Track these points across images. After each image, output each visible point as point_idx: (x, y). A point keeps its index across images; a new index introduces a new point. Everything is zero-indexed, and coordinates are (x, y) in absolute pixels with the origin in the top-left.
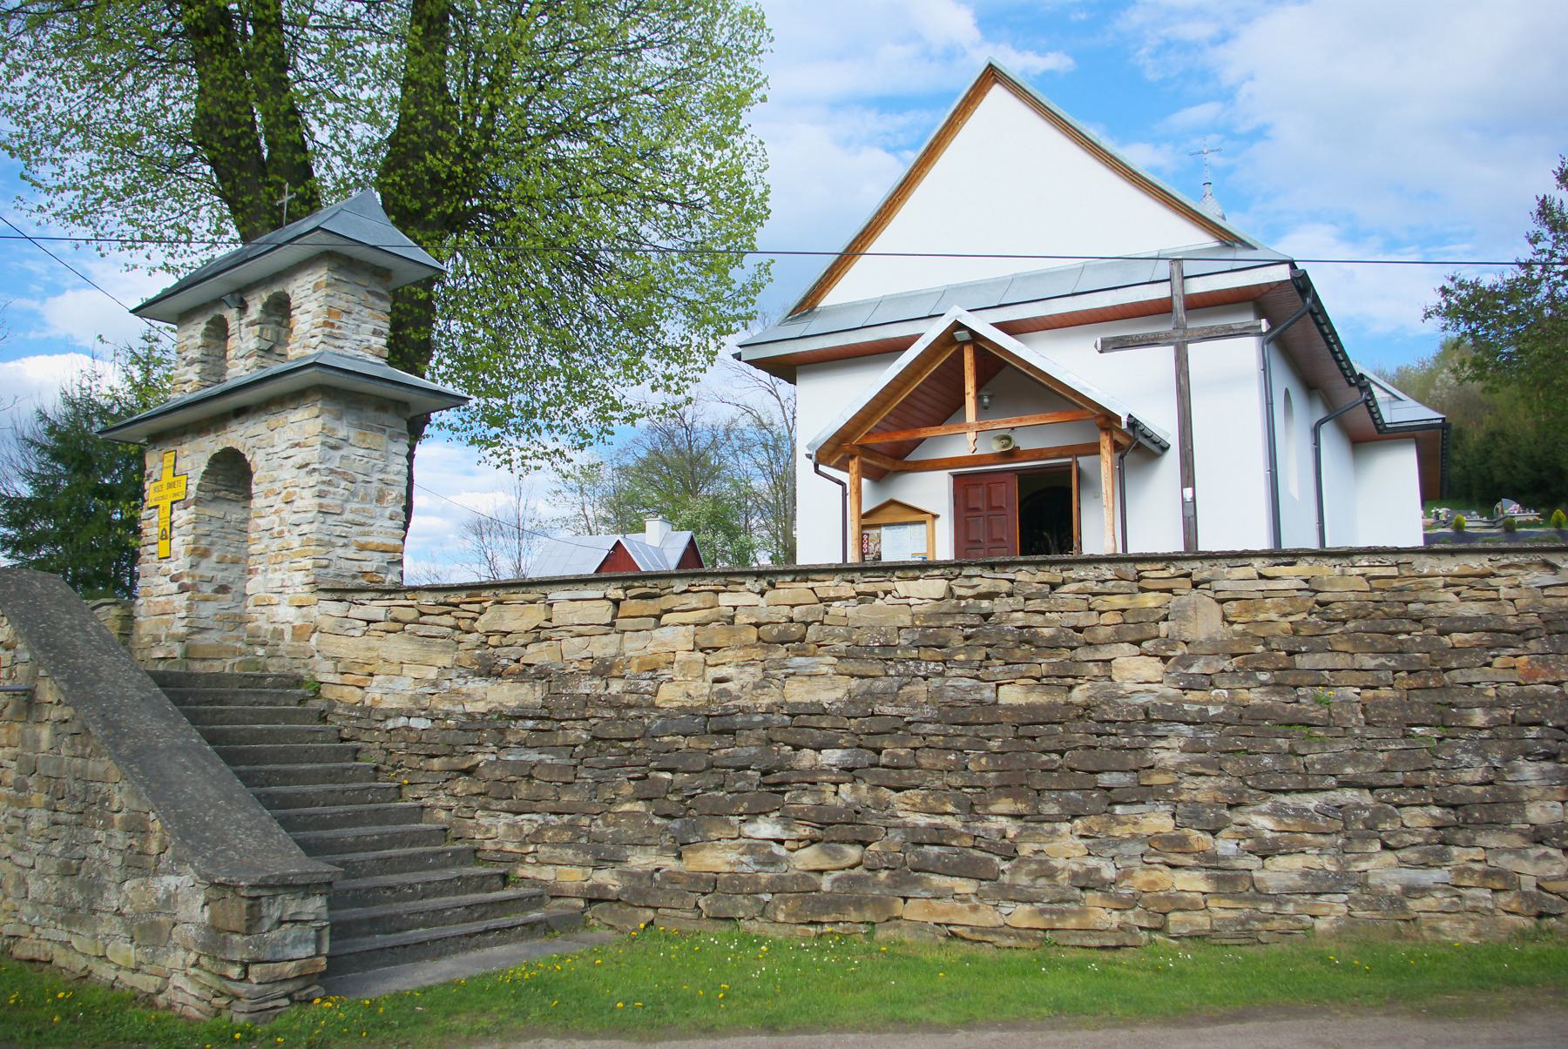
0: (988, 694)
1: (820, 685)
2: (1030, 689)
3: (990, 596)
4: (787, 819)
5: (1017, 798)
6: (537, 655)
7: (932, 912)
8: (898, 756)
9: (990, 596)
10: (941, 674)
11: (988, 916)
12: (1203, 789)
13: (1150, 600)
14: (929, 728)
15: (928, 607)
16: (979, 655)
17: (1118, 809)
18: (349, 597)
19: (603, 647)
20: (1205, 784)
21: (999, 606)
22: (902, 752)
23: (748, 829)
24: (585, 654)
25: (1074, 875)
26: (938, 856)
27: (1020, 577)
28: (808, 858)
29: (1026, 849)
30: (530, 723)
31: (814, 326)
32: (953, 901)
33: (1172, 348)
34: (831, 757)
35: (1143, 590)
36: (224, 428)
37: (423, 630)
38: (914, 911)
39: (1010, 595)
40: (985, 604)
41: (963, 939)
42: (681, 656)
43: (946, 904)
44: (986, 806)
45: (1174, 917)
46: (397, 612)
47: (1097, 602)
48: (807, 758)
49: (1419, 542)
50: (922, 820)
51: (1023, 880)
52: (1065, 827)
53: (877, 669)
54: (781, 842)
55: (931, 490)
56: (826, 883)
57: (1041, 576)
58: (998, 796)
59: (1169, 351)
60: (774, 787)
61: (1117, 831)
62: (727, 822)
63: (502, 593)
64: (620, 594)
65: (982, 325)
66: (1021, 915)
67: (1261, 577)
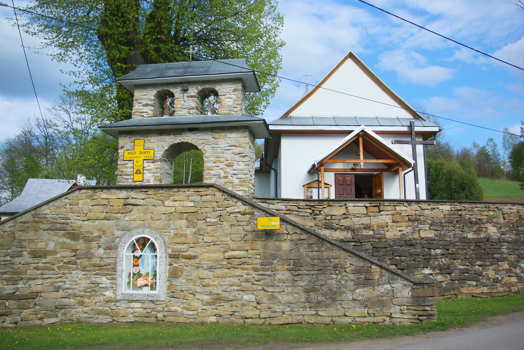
0: (465, 235)
1: (428, 233)
2: (474, 234)
3: (460, 210)
4: (433, 268)
5: (481, 261)
6: (343, 222)
7: (468, 290)
8: (453, 251)
9: (460, 210)
10: (454, 230)
11: (479, 291)
12: (512, 258)
13: (491, 213)
14: (458, 244)
15: (446, 213)
16: (461, 226)
17: (499, 263)
18: (268, 201)
19: (365, 221)
20: (512, 257)
21: (463, 213)
22: (454, 250)
23: (423, 272)
24: (361, 223)
25: (494, 279)
26: (468, 276)
27: (466, 206)
28: (439, 278)
29: (484, 273)
30: (353, 243)
31: (288, 122)
32: (470, 288)
33: (417, 145)
34: (439, 251)
35: (490, 210)
36: (181, 134)
37: (301, 214)
38: (464, 290)
39: (464, 210)
40: (460, 212)
41: (476, 297)
42: (389, 224)
43: (471, 288)
44: (475, 263)
45: (512, 288)
46: (289, 207)
47: (482, 213)
48: (433, 252)
49: (302, 198)
50: (462, 267)
51: (485, 281)
52: (490, 268)
53: (440, 228)
54: (431, 274)
55: (329, 178)
56: (444, 285)
57: (470, 206)
58: (477, 260)
59: (410, 146)
60: (427, 261)
61: (500, 268)
62: (418, 270)
63: (331, 203)
64: (369, 205)
65: (369, 131)
66: (485, 290)
67: (510, 209)
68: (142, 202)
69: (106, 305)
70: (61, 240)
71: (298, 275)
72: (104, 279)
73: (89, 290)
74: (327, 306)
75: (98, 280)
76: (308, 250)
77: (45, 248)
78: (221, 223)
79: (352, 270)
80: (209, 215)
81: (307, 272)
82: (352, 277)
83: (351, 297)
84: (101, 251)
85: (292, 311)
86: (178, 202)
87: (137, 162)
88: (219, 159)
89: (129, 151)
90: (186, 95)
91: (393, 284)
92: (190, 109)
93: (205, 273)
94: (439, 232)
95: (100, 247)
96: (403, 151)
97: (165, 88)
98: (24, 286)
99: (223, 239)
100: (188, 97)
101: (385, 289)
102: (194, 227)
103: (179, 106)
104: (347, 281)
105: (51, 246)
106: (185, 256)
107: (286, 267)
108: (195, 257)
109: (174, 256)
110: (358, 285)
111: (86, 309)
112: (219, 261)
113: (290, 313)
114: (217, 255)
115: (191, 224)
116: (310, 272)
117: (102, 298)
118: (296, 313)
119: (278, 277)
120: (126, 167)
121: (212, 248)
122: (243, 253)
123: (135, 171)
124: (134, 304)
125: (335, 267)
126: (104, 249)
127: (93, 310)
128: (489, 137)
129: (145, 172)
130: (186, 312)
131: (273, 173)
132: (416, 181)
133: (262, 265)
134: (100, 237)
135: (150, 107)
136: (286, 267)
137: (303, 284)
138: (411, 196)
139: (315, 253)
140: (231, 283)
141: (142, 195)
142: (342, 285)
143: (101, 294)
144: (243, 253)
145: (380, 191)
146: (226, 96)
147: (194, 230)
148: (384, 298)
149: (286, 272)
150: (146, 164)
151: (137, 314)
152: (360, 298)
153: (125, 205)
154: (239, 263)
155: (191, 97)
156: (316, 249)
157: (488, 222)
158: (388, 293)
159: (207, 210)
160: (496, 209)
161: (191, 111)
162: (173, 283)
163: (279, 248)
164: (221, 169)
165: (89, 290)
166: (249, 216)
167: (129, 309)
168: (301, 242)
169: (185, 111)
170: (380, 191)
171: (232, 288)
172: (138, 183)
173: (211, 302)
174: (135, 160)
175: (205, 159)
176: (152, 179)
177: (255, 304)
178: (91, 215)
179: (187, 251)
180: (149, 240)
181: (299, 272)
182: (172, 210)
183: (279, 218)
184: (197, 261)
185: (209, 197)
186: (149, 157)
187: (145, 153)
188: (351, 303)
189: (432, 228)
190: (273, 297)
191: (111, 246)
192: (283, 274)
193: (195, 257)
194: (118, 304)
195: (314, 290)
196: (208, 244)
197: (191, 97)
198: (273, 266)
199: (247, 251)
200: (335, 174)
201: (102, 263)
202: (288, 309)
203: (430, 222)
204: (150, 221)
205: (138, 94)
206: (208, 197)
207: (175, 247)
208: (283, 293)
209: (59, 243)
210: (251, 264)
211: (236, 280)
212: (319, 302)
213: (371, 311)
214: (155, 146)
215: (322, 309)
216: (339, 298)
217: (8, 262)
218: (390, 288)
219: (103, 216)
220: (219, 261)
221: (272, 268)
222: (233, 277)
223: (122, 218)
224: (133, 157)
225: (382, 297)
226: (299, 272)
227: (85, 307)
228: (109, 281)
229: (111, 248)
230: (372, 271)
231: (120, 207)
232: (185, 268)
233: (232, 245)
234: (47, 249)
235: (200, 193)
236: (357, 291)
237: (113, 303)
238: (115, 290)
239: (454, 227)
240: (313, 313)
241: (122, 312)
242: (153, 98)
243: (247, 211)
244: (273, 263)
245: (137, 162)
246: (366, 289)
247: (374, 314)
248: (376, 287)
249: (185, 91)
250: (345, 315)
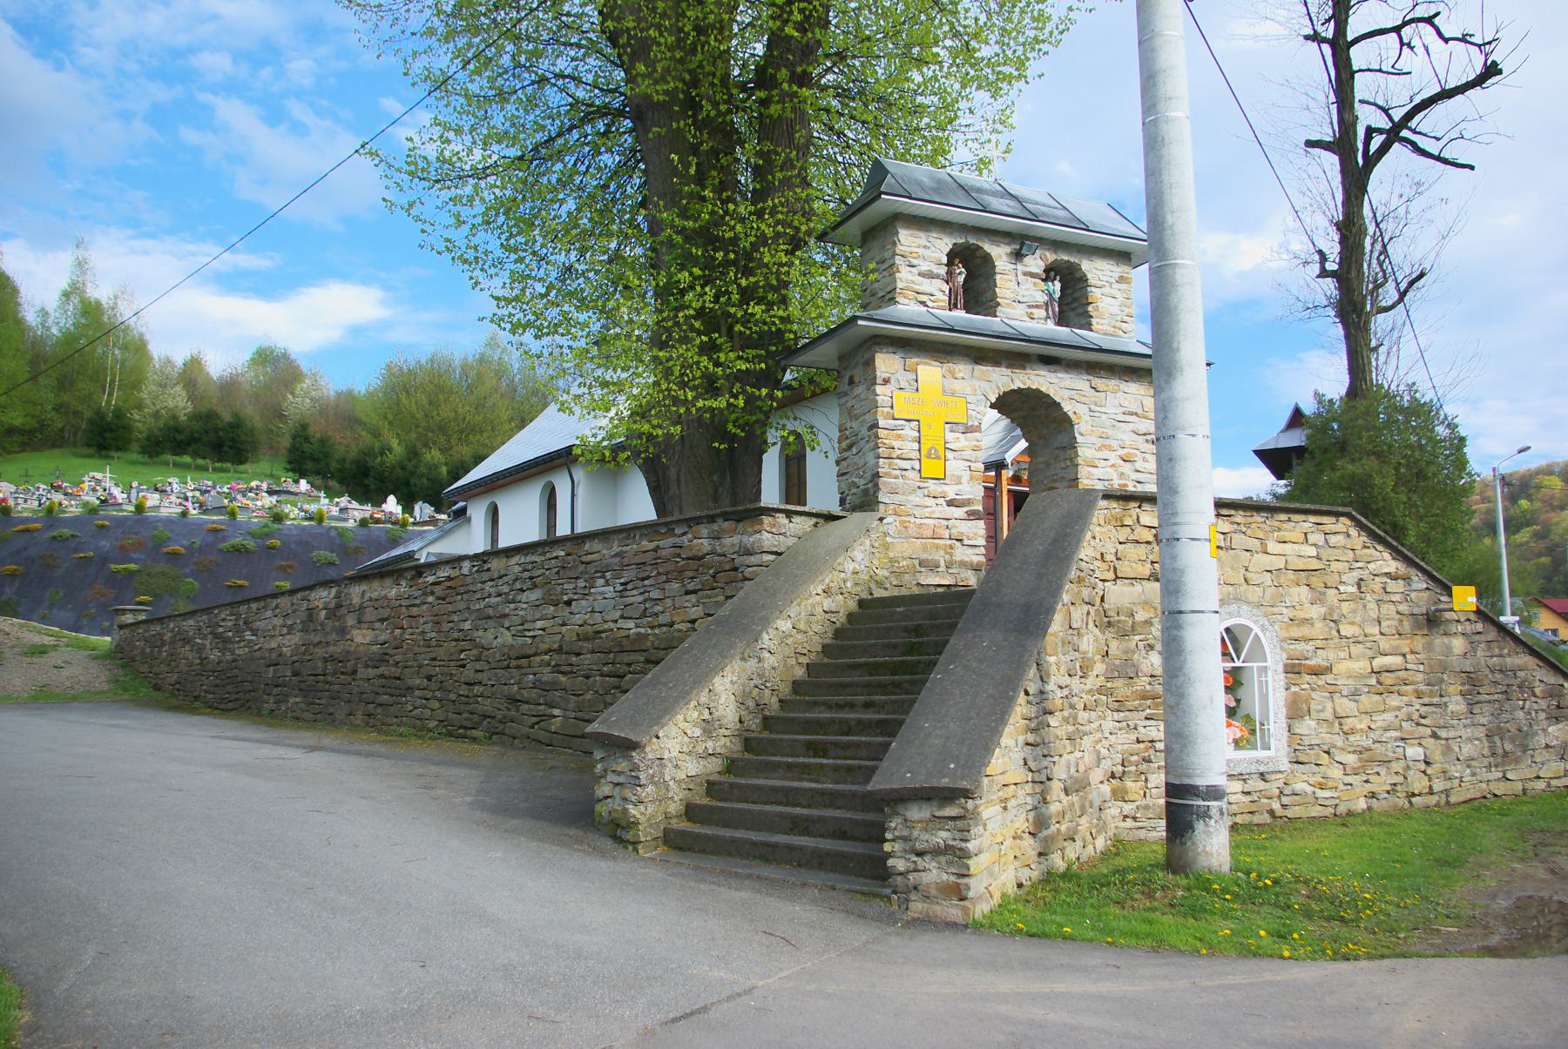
73: (1134, 758)
74: (1517, 761)
80: (1344, 578)
82: (1543, 704)
85: (1473, 774)
86: (1290, 546)
88: (1107, 442)
90: (1020, 267)
93: (1345, 706)
97: (972, 241)
100: (1025, 274)
103: (1008, 294)
106: (1310, 667)
108: (1329, 669)
109: (1293, 669)
120: (899, 436)
130: (1320, 793)
155: (1032, 275)
156: (1497, 651)
162: (1297, 731)
163: (1449, 648)
165: (1134, 758)
169: (1020, 311)
171: (1389, 734)
175: (1079, 439)
182: (1279, 563)
184: (1329, 678)
185: (1340, 538)
197: (1032, 275)
205: (907, 239)
214: (968, 390)
232: (1314, 695)
233: (1384, 644)
249: (1018, 256)
250: (1538, 777)
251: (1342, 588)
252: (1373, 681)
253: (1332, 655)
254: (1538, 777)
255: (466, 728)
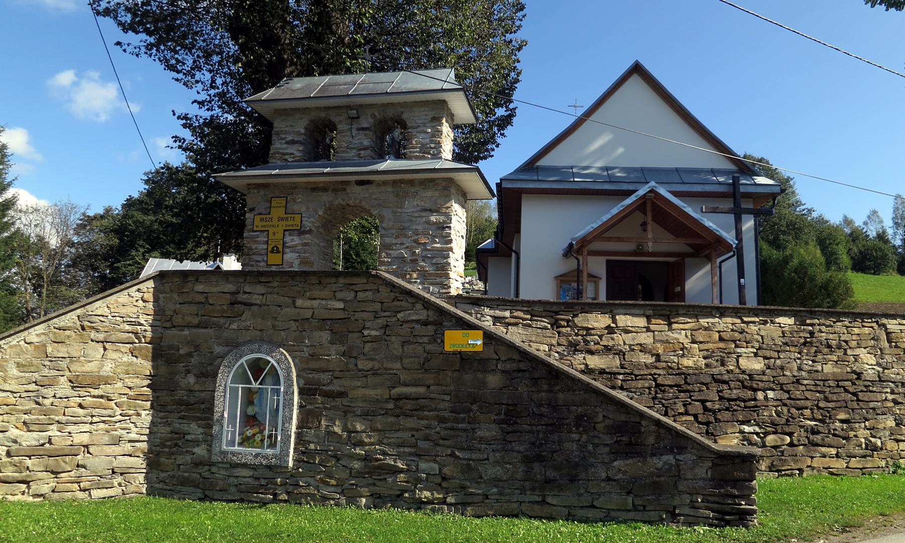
35: (864, 326)
65: (663, 191)
68: (256, 299)
69: (194, 470)
70: (125, 359)
71: (514, 432)
72: (194, 426)
73: (169, 443)
74: (561, 488)
75: (185, 428)
76: (531, 389)
77: (99, 372)
78: (387, 338)
79: (607, 427)
81: (529, 428)
82: (608, 440)
83: (604, 475)
84: (191, 379)
85: (501, 494)
86: (319, 301)
87: (274, 234)
89: (262, 216)
91: (679, 454)
92: (361, 150)
94: (773, 360)
95: (189, 372)
96: (718, 224)
98: (60, 434)
99: (389, 365)
100: (358, 130)
101: (665, 463)
102: (342, 343)
104: (597, 445)
105: (108, 368)
107: (493, 417)
108: (342, 394)
110: (618, 452)
111: (162, 475)
112: (381, 402)
113: (497, 497)
114: (379, 391)
115: (338, 338)
116: (534, 428)
117: (188, 458)
118: (507, 497)
119: (480, 433)
120: (256, 242)
121: (370, 380)
122: (421, 390)
123: (270, 249)
124: (239, 470)
125: (579, 418)
126: (195, 375)
127: (173, 477)
128: (872, 208)
129: (287, 250)
131: (513, 254)
132: (741, 274)
133: (452, 412)
134: (190, 355)
135: (296, 146)
136: (493, 417)
137: (521, 448)
138: (732, 301)
139: (543, 394)
140: (400, 441)
141: (260, 289)
142: (589, 452)
143: (187, 452)
144: (421, 390)
145: (678, 289)
146: (419, 129)
147: (342, 349)
148: (662, 479)
149: (493, 426)
150: (288, 239)
151: (243, 487)
152: (620, 476)
153: (232, 304)
154: (414, 408)
156: (545, 387)
157: (859, 346)
158: (670, 470)
159: (365, 315)
160: (874, 325)
161: (362, 152)
163: (484, 383)
164: (407, 247)
165: (169, 443)
166: (435, 328)
167: (232, 479)
168: (520, 375)
170: (678, 289)
172: (274, 269)
173: (365, 473)
174: (271, 230)
176: (297, 262)
177: (439, 480)
178: (178, 320)
179: (328, 384)
180: (269, 362)
181: (516, 427)
183: (481, 332)
184: (345, 401)
185: (369, 294)
186: (292, 226)
187: (287, 219)
188: (603, 484)
189: (760, 353)
190: (467, 469)
191: (207, 372)
192: (488, 430)
193: (342, 394)
194: (214, 469)
195: (539, 458)
196: (365, 374)
197: (363, 129)
198: (472, 414)
199: (429, 387)
200: (608, 261)
201: (192, 400)
202: (495, 490)
203: (757, 345)
204: (271, 331)
206: (367, 293)
207: (310, 376)
208: (486, 462)
209: (124, 364)
210: (435, 410)
211: (406, 435)
212: (548, 481)
213: (638, 502)
215: (553, 493)
216: (583, 475)
217: (34, 394)
218: (673, 461)
219: (196, 321)
220: (381, 402)
221: (470, 417)
222: (403, 430)
223: (227, 326)
224: (268, 226)
225: (658, 477)
226: (516, 427)
227: (162, 471)
228: (201, 430)
229: (209, 375)
230: (643, 429)
231: (225, 307)
234: (101, 374)
235: (354, 287)
236: (616, 463)
237: (207, 468)
238: (210, 446)
239: (799, 353)
240: (537, 499)
241: (220, 482)
242: (303, 131)
243: (430, 319)
244: (471, 410)
245: (274, 234)
246: (630, 461)
247: (644, 507)
248: (649, 459)
251: (366, 332)
252: (391, 406)
253: (346, 383)
254: (593, 506)
255: (519, 371)
